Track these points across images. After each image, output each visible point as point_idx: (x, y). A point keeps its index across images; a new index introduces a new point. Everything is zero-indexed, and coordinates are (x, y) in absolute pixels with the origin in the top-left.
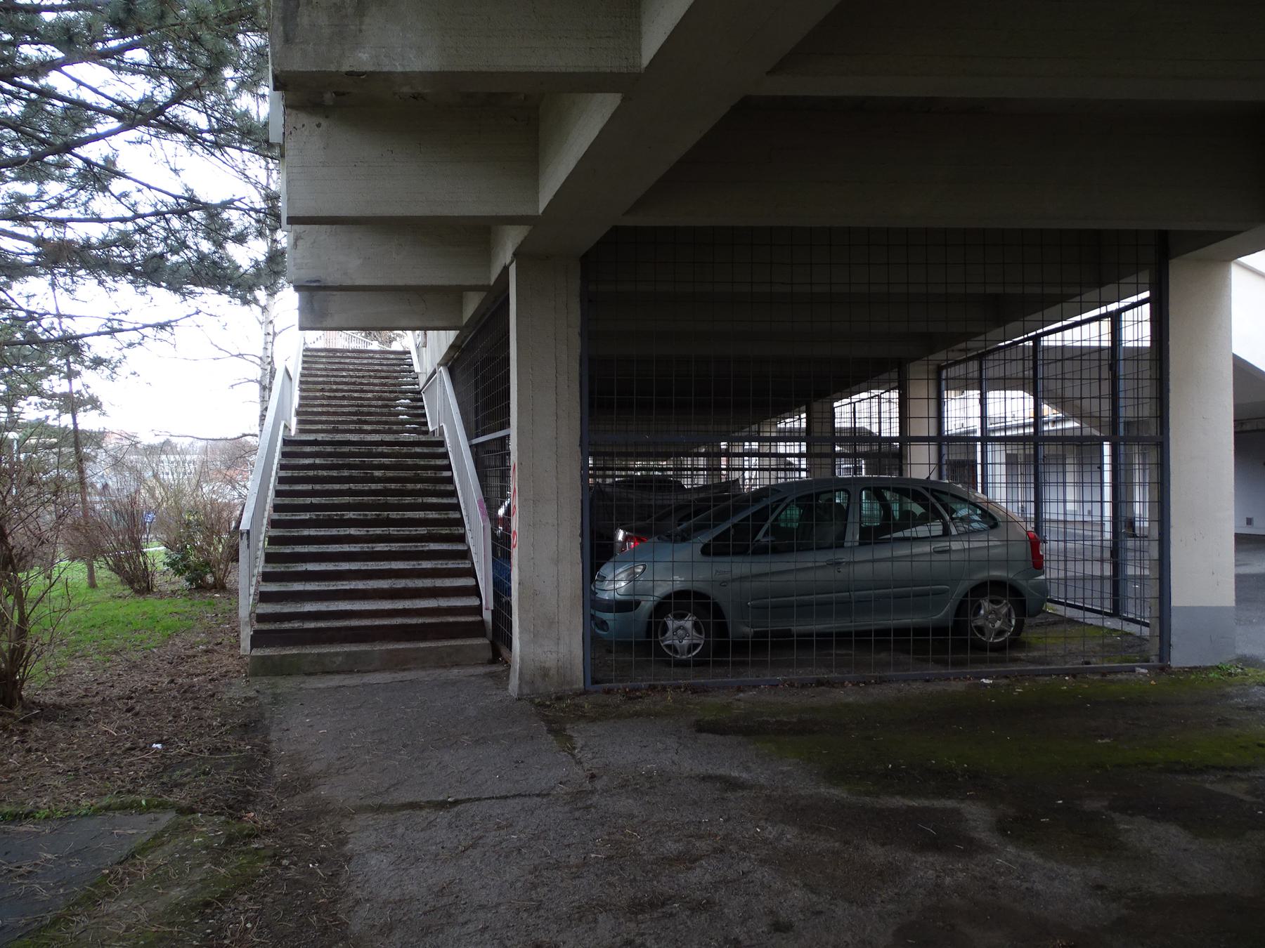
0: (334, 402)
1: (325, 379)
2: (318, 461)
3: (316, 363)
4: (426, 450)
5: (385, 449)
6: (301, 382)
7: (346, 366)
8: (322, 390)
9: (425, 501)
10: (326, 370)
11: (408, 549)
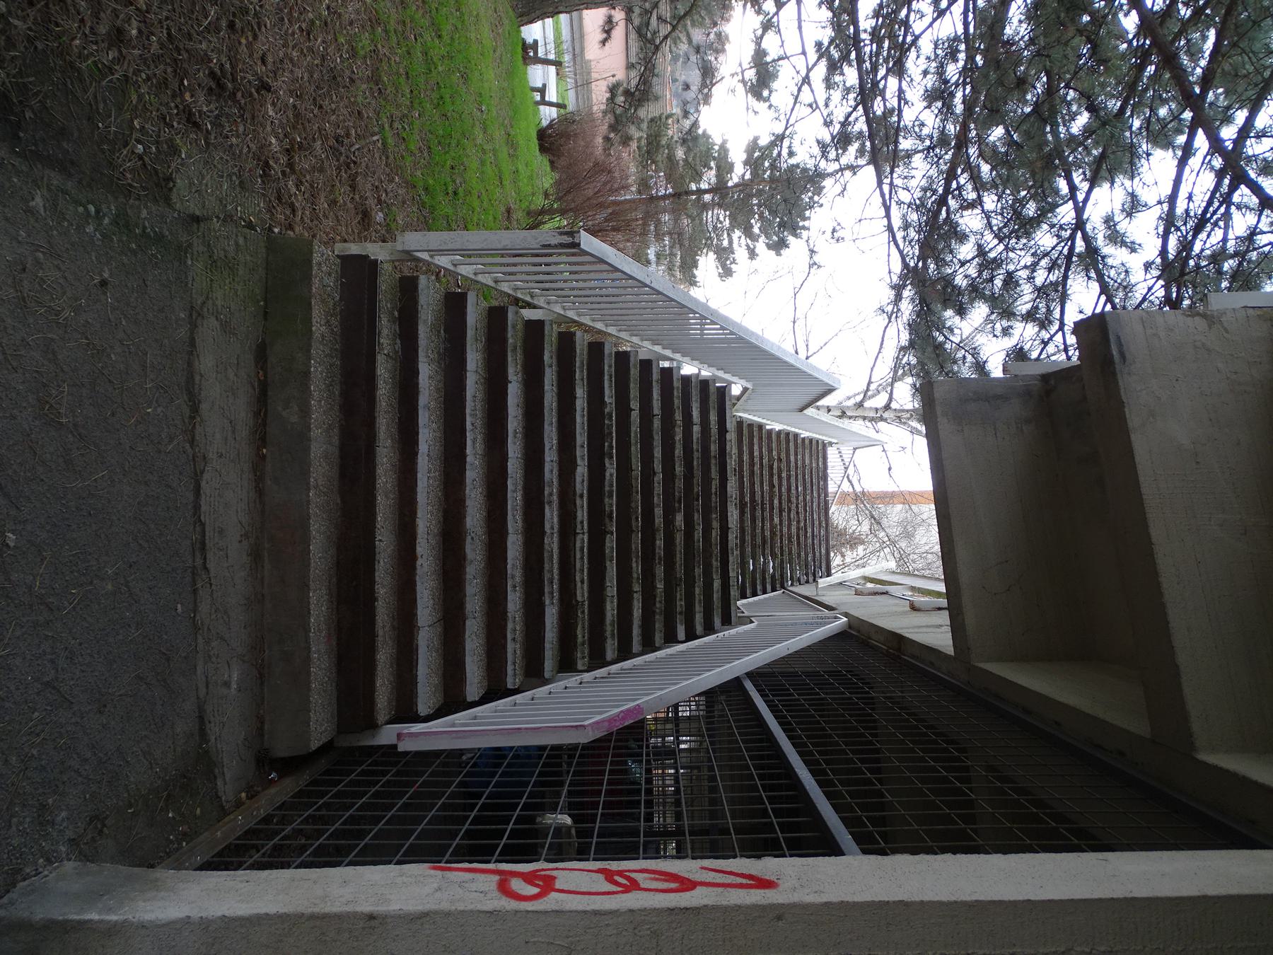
0: (766, 472)
1: (793, 464)
2: (696, 429)
3: (811, 456)
4: (716, 596)
5: (716, 534)
6: (788, 434)
7: (809, 492)
8: (780, 460)
9: (635, 595)
10: (804, 466)
11: (547, 566)
